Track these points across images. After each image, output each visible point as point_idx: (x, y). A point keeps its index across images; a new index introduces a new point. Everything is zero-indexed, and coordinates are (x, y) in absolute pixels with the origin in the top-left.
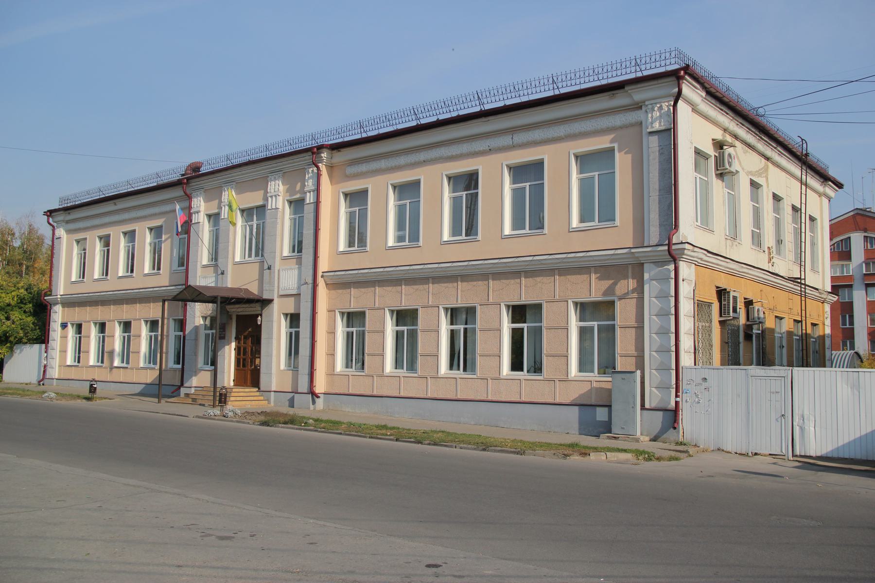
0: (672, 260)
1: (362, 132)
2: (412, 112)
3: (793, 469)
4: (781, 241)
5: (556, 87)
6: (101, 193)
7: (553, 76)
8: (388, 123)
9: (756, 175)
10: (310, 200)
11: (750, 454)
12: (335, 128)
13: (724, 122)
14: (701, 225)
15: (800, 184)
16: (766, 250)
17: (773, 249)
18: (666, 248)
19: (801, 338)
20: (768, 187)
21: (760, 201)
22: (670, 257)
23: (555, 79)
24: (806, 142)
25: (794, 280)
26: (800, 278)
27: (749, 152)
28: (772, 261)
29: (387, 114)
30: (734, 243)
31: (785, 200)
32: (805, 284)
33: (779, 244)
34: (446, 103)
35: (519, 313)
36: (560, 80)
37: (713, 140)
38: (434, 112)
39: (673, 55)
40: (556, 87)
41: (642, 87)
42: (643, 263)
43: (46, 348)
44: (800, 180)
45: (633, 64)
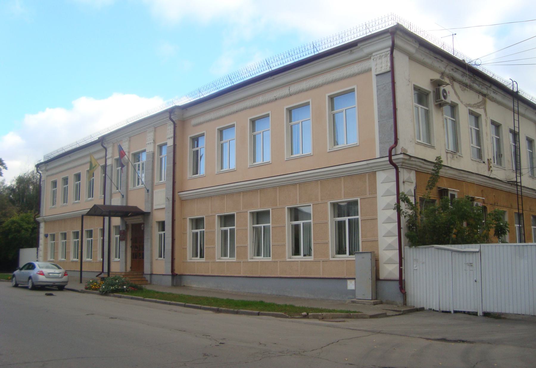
0: (393, 167)
1: (200, 95)
2: (228, 78)
4: (501, 155)
7: (313, 42)
9: (475, 107)
10: (516, 192)
11: (452, 312)
12: (212, 83)
13: (478, 78)
14: (423, 142)
15: (513, 112)
16: (486, 161)
17: (491, 161)
18: (387, 159)
19: (523, 226)
20: (486, 115)
21: (480, 126)
22: (391, 166)
23: (315, 45)
24: (517, 83)
25: (510, 183)
26: (516, 182)
27: (467, 91)
28: (491, 169)
29: (213, 82)
30: (454, 156)
31: (503, 126)
32: (521, 186)
33: (500, 157)
34: (248, 69)
35: (296, 213)
36: (318, 45)
38: (241, 77)
39: (390, 19)
41: (370, 43)
42: (376, 171)
43: (37, 250)
44: (513, 109)
45: (364, 28)
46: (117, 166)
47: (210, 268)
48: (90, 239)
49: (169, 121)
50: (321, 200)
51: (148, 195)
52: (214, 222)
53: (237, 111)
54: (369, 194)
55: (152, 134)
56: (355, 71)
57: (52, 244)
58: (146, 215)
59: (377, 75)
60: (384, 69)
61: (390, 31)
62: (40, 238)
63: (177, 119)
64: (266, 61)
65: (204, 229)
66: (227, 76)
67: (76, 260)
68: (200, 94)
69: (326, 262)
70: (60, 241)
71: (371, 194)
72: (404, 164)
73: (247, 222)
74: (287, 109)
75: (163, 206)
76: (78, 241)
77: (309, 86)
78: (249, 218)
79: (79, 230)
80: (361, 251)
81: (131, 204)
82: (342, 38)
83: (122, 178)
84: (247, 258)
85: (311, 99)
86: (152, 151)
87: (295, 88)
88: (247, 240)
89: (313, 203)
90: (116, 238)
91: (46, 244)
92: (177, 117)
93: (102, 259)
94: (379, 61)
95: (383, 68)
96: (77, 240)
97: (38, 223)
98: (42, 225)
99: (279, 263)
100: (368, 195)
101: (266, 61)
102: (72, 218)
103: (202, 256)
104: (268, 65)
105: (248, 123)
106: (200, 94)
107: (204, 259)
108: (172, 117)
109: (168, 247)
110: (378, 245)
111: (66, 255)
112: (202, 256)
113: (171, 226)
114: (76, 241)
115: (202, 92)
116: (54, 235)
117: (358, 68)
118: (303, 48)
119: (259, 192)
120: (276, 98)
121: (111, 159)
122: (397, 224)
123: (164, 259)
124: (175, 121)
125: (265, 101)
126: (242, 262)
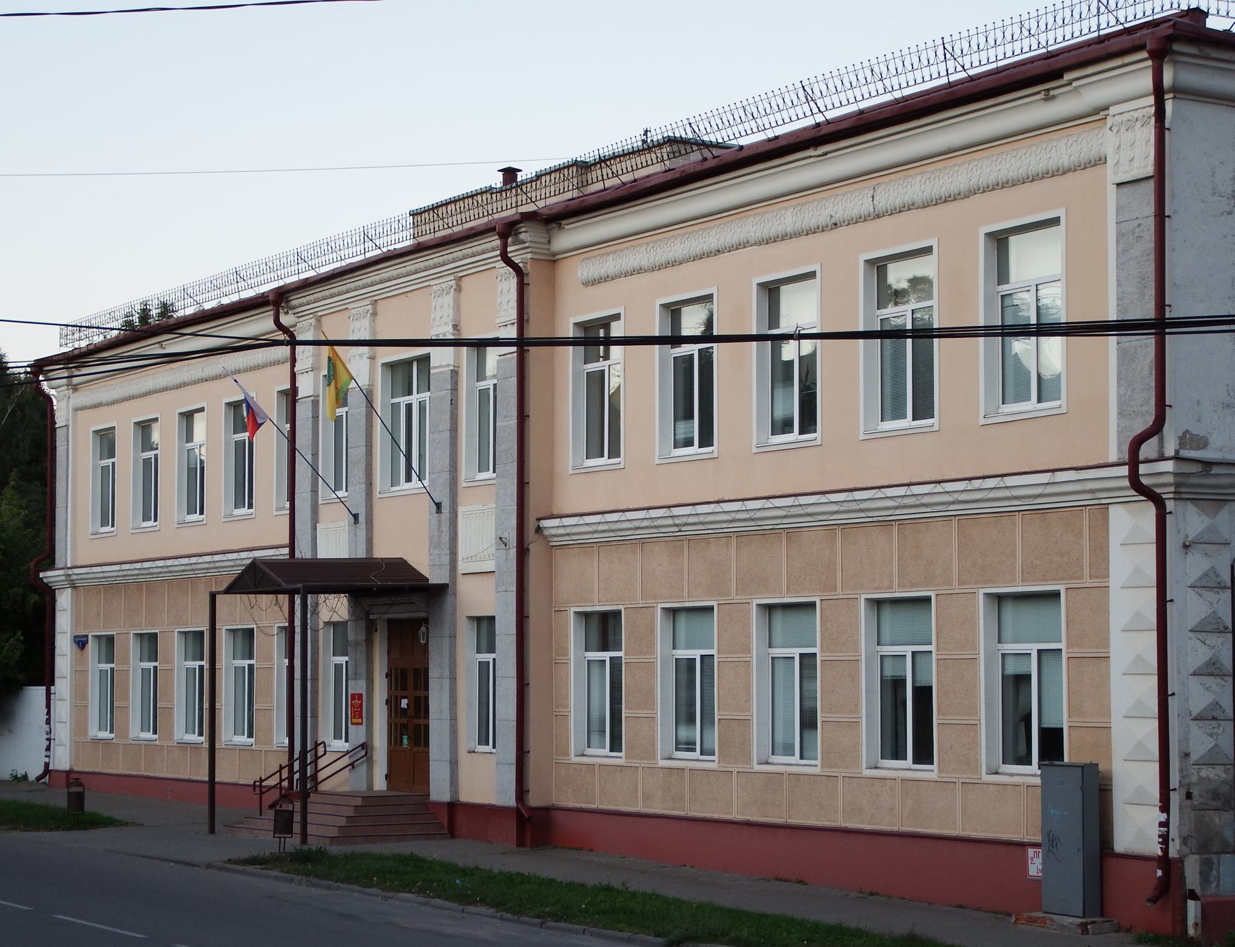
3: (117, 815)
5: (815, 110)
6: (242, 284)
8: (880, 85)
12: (1017, 19)
18: (1124, 471)
34: (876, 69)
37: (1059, 217)
40: (815, 110)
46: (101, 458)
47: (640, 787)
48: (151, 665)
49: (512, 257)
50: (961, 583)
51: (440, 521)
52: (652, 632)
53: (719, 251)
54: (1022, 581)
55: (449, 299)
56: (1061, 162)
57: (145, 672)
58: (435, 594)
59: (1119, 185)
60: (1138, 169)
61: (271, 298)
62: (57, 651)
63: (529, 256)
64: (803, 87)
65: (157, 661)
66: (686, 122)
67: (194, 738)
68: (951, 64)
69: (971, 786)
70: (134, 665)
71: (1096, 577)
72: (1183, 490)
73: (749, 636)
74: (989, 235)
75: (489, 566)
76: (201, 668)
77: (1077, 156)
78: (863, 622)
79: (205, 627)
80: (1066, 759)
81: (383, 551)
82: (219, 289)
83: (349, 450)
84: (749, 760)
85: (1064, 209)
86: (448, 365)
87: (893, 192)
88: (748, 701)
89: (1068, 586)
90: (338, 667)
91: (79, 674)
92: (529, 250)
93: (286, 741)
94: (1126, 137)
95: (1136, 163)
96: (197, 664)
97: (49, 594)
98: (64, 600)
99: (840, 780)
100: (1087, 582)
101: (803, 87)
102: (181, 582)
103: (924, 754)
104: (812, 103)
105: (981, 250)
106: (951, 64)
107: (935, 767)
108: (509, 249)
109: (506, 709)
110: (1109, 740)
111: (154, 718)
112: (924, 754)
113: (514, 638)
114: (107, 670)
115: (340, 250)
116: (110, 640)
117: (836, 208)
118: (820, 83)
119: (784, 540)
120: (833, 221)
121: (311, 374)
122: (1154, 680)
123: (494, 751)
124: (521, 265)
125: (1028, 174)
126: (735, 774)
